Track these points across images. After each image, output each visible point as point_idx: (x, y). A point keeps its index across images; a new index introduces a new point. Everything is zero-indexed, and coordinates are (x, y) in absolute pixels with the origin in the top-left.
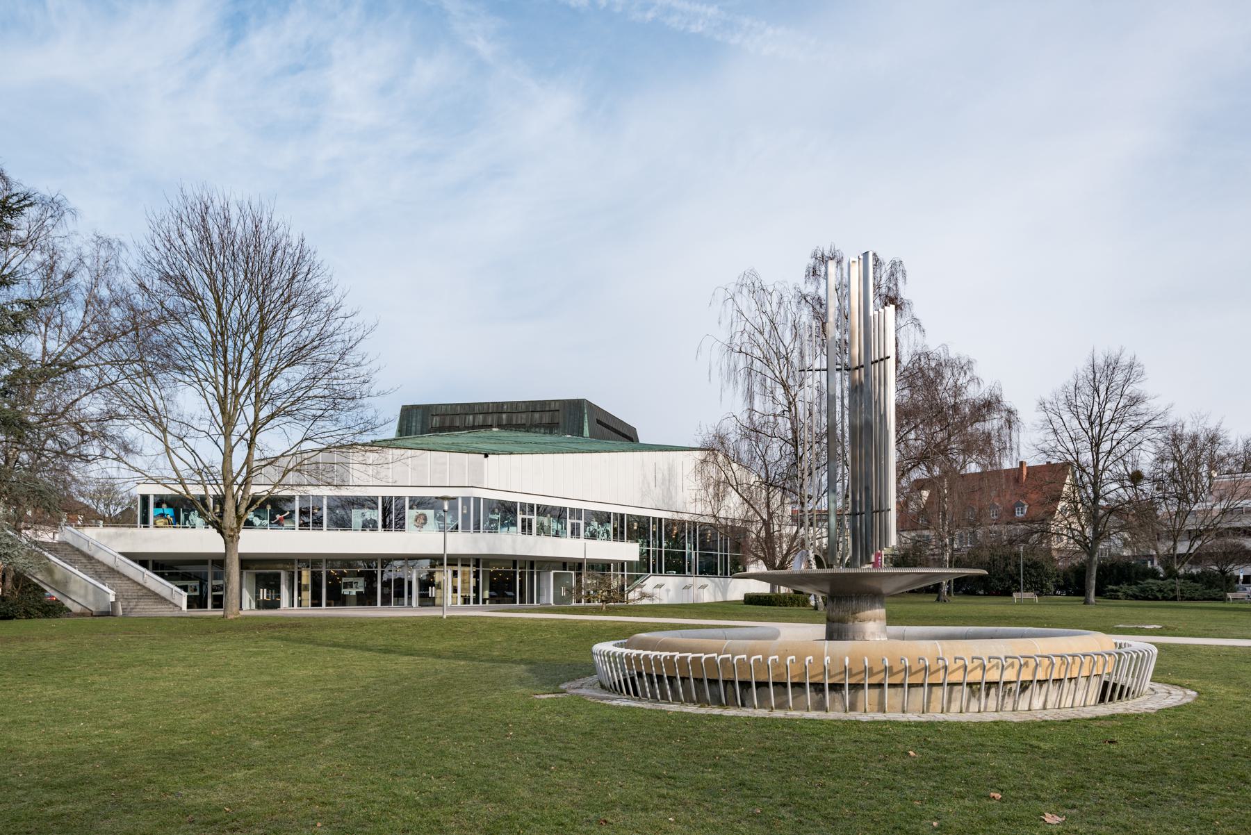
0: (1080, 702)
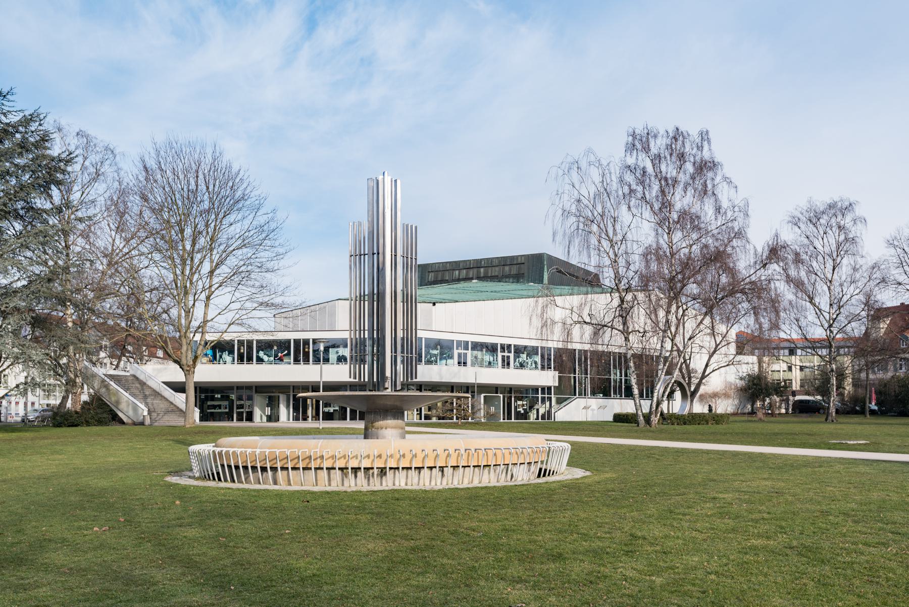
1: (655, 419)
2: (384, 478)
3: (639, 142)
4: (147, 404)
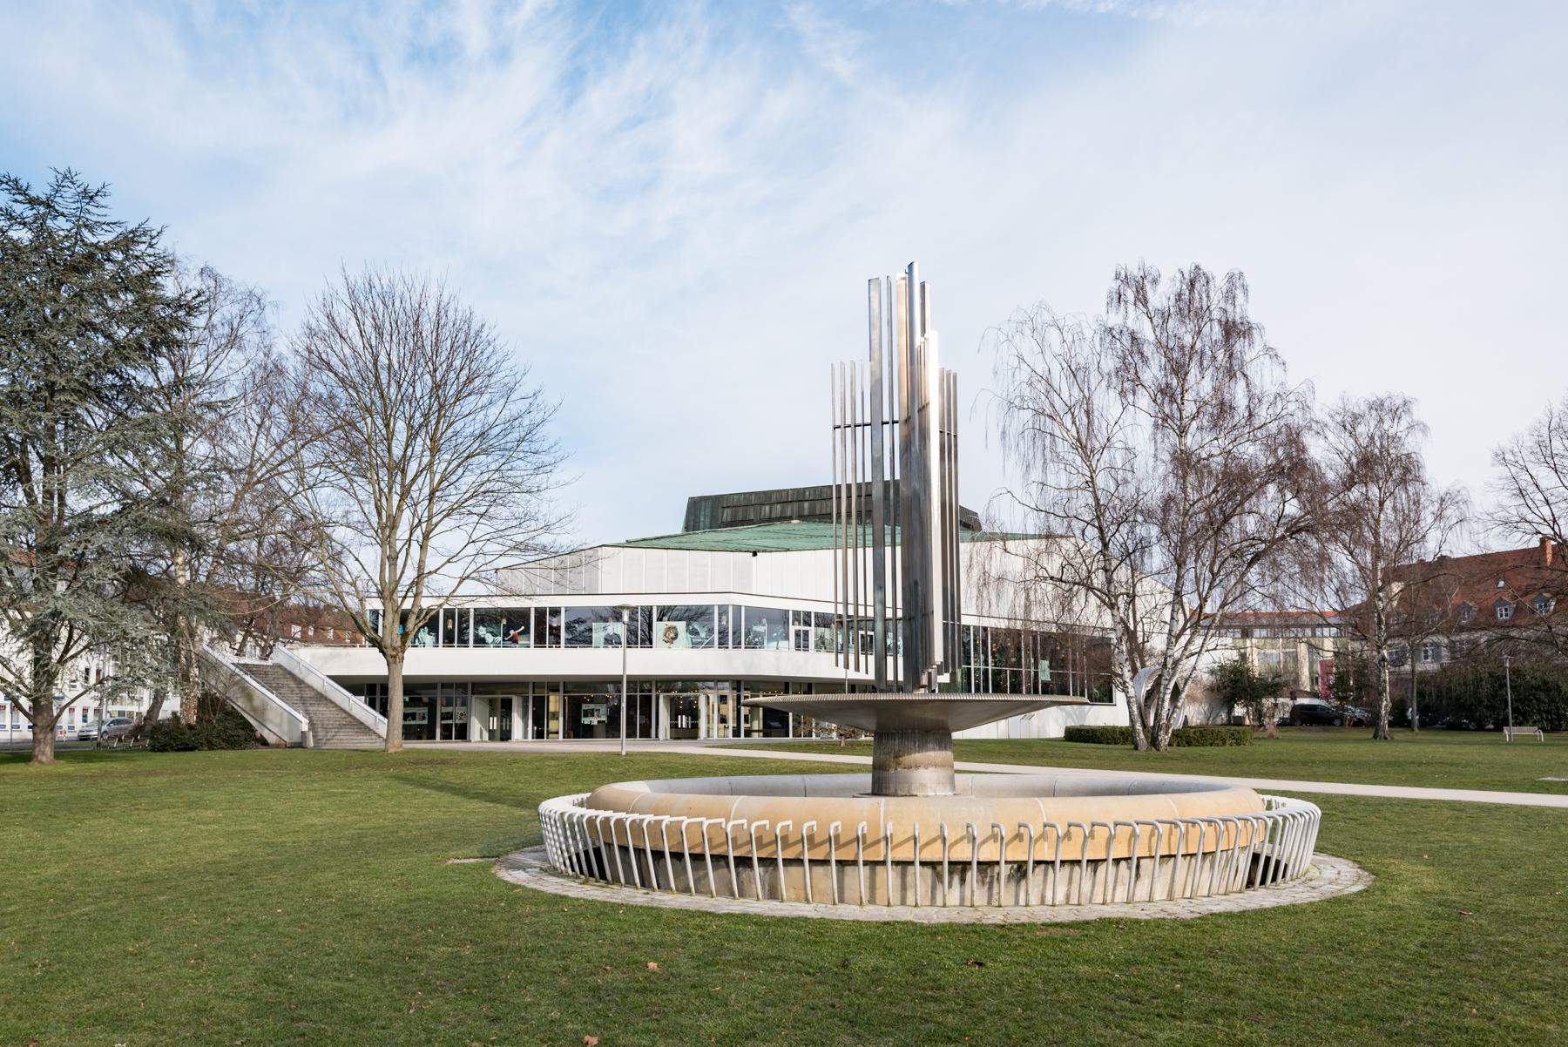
0: (1212, 892)
1: (1165, 738)
2: (1023, 883)
3: (1135, 288)
4: (307, 713)
